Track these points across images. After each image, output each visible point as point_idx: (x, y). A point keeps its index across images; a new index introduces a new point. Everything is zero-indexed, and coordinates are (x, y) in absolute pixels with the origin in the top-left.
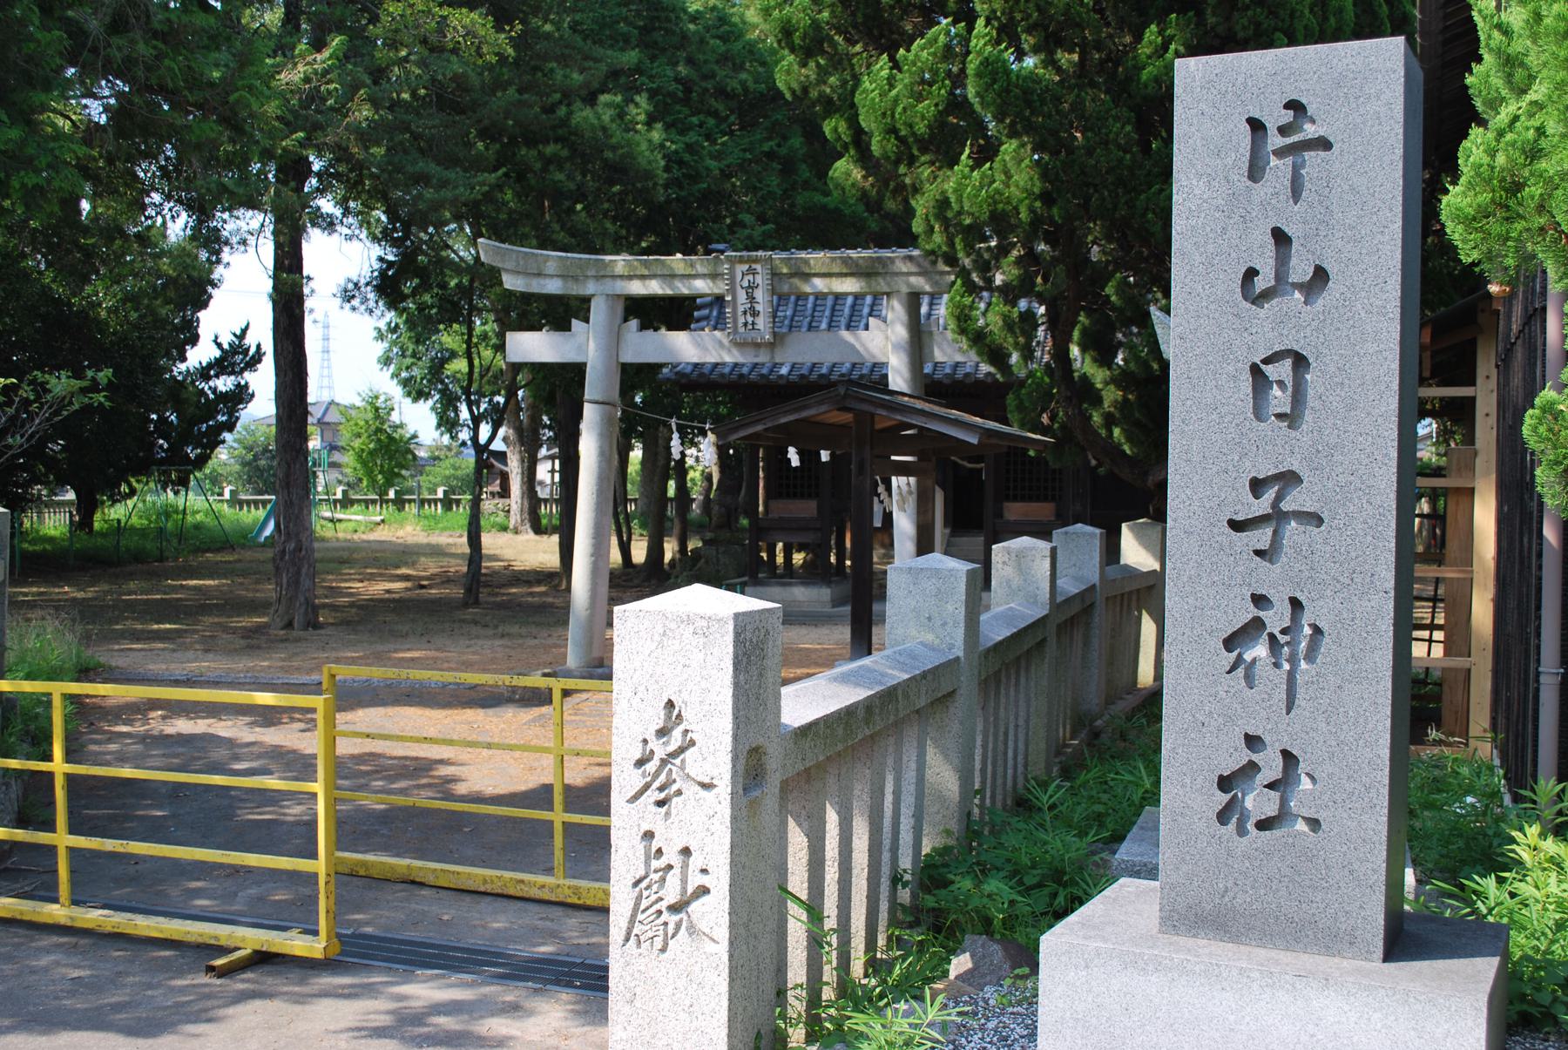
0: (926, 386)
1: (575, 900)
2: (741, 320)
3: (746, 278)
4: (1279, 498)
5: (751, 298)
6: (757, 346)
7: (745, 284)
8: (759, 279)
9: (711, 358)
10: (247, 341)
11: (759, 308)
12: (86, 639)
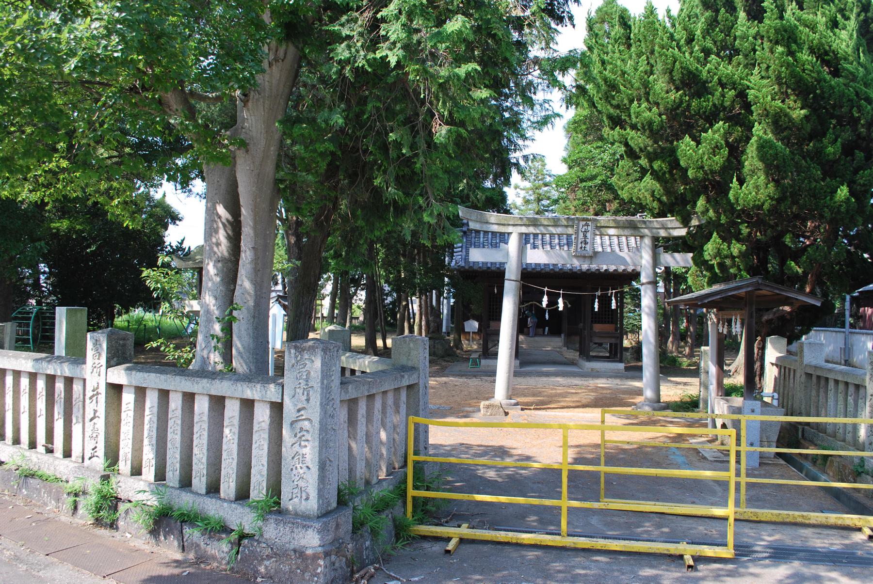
0: (522, 274)
1: (755, 519)
2: (580, 246)
5: (585, 236)
8: (589, 228)
9: (560, 262)
10: (184, 246)
12: (646, 398)
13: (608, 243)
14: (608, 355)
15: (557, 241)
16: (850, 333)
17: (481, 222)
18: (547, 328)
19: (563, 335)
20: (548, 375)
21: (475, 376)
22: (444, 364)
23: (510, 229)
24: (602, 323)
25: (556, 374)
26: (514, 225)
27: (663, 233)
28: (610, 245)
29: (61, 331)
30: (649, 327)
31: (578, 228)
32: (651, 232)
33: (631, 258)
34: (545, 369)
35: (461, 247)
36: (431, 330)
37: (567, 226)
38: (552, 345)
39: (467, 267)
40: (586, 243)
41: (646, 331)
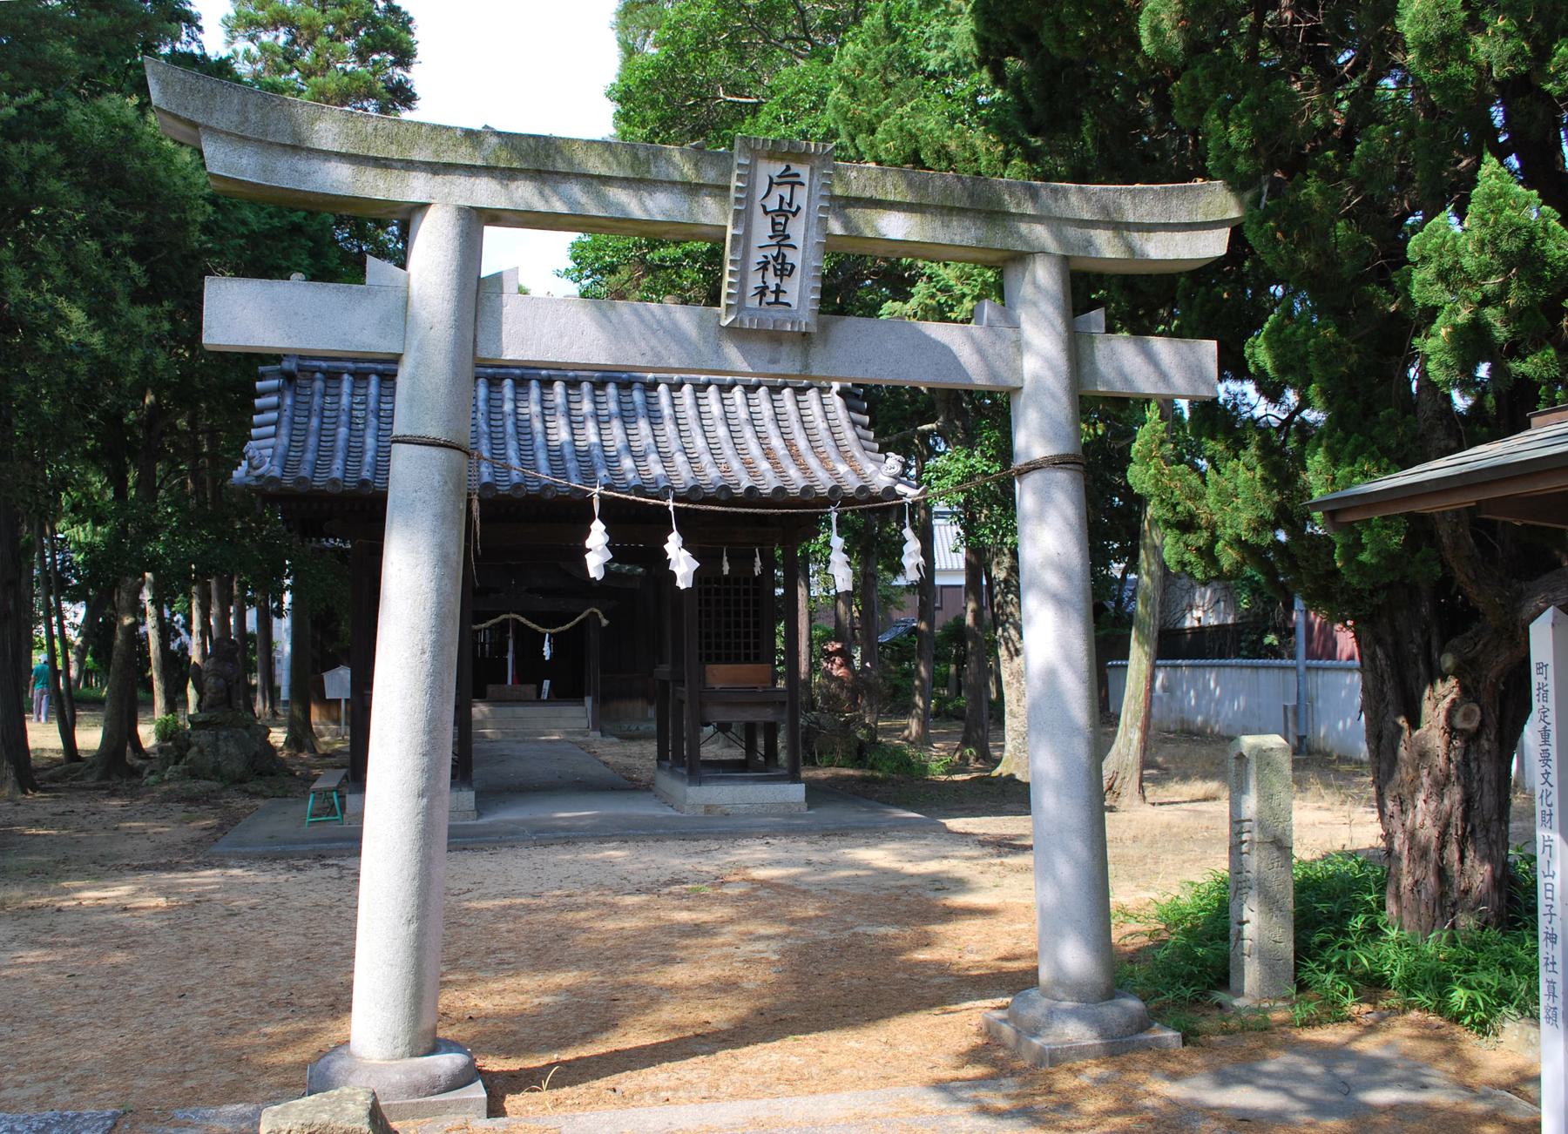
2: (755, 281)
3: (777, 192)
4: (1355, 1038)
5: (781, 237)
6: (775, 337)
7: (773, 204)
11: (794, 257)
13: (743, 414)
14: (738, 753)
15: (587, 406)
16: (1308, 668)
17: (263, 144)
18: (546, 684)
19: (588, 701)
20: (571, 836)
21: (320, 857)
22: (239, 803)
23: (416, 188)
24: (728, 660)
25: (601, 834)
26: (437, 168)
27: (1107, 247)
28: (751, 421)
29: (1138, 672)
30: (1068, 659)
31: (749, 189)
32: (1060, 239)
33: (980, 351)
34: (566, 813)
35: (276, 423)
36: (207, 698)
37: (692, 189)
38: (559, 727)
39: (288, 482)
40: (784, 270)
41: (1050, 676)
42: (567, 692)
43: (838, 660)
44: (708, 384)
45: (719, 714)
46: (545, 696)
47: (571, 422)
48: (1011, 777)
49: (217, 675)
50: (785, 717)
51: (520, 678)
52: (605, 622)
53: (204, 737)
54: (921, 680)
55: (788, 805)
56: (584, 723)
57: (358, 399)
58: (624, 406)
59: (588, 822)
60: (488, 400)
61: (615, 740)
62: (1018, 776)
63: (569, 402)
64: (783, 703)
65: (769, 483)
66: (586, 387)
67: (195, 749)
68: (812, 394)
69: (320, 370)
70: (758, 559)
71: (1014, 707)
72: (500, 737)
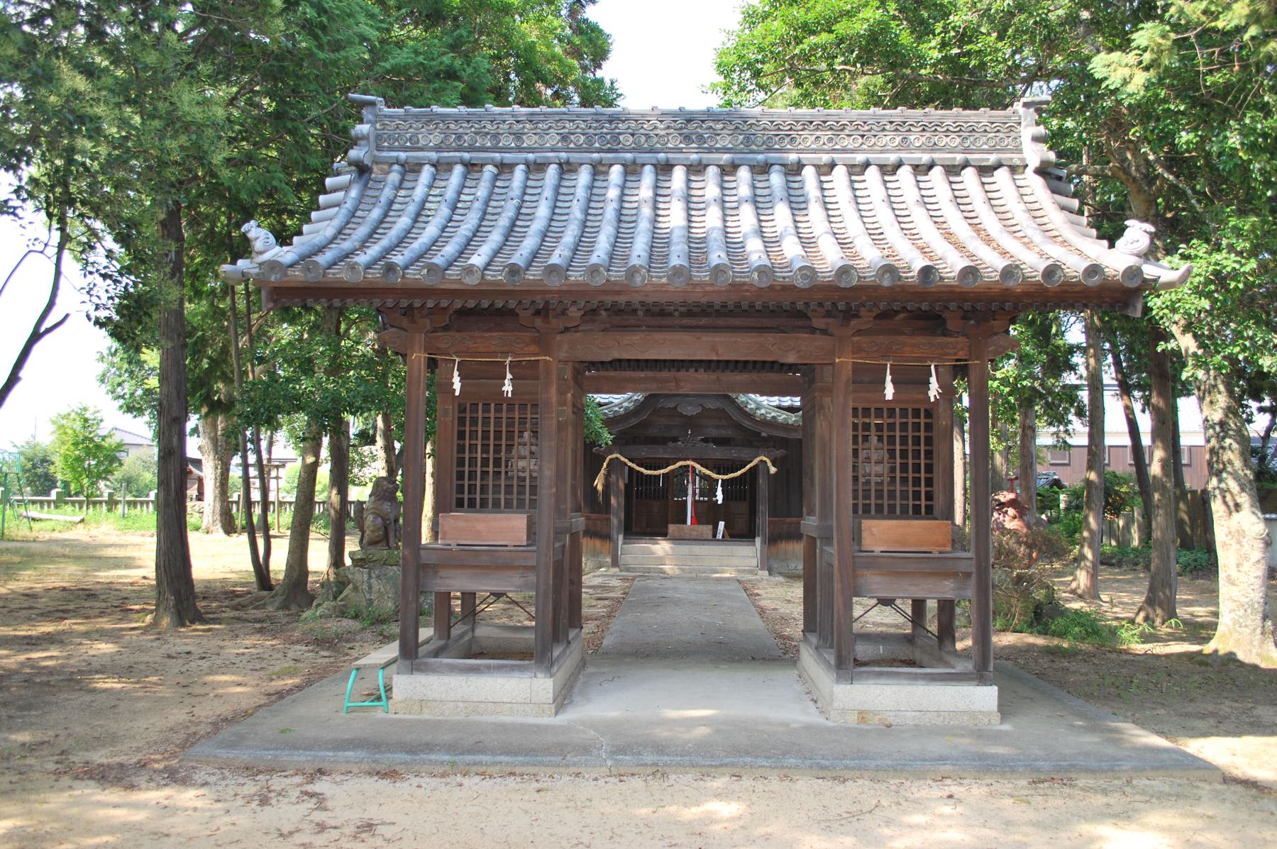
18: (722, 524)
19: (758, 540)
24: (892, 514)
42: (741, 533)
43: (1011, 511)
44: (867, 165)
45: (876, 582)
46: (719, 536)
47: (689, 209)
48: (1231, 658)
49: (377, 515)
50: (971, 592)
51: (697, 520)
52: (773, 470)
53: (360, 576)
54: (1090, 531)
55: (973, 714)
56: (754, 562)
57: (437, 191)
58: (759, 192)
59: (702, 731)
60: (591, 187)
61: (781, 579)
62: (1241, 656)
63: (689, 188)
64: (968, 575)
65: (952, 264)
66: (712, 171)
67: (351, 586)
68: (1002, 175)
69: (397, 162)
70: (933, 380)
71: (1234, 574)
72: (677, 572)
